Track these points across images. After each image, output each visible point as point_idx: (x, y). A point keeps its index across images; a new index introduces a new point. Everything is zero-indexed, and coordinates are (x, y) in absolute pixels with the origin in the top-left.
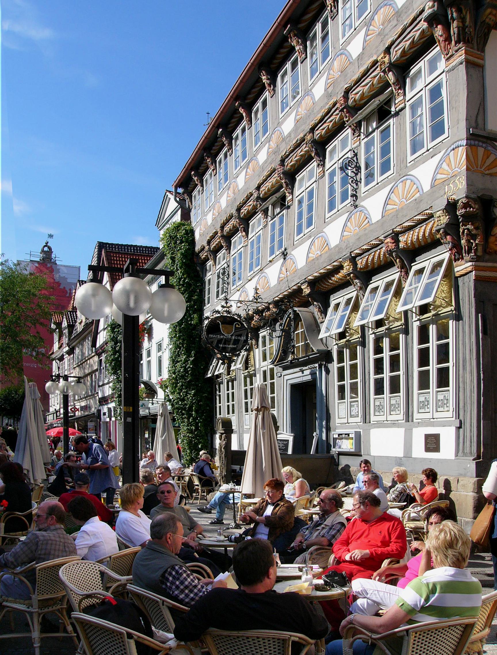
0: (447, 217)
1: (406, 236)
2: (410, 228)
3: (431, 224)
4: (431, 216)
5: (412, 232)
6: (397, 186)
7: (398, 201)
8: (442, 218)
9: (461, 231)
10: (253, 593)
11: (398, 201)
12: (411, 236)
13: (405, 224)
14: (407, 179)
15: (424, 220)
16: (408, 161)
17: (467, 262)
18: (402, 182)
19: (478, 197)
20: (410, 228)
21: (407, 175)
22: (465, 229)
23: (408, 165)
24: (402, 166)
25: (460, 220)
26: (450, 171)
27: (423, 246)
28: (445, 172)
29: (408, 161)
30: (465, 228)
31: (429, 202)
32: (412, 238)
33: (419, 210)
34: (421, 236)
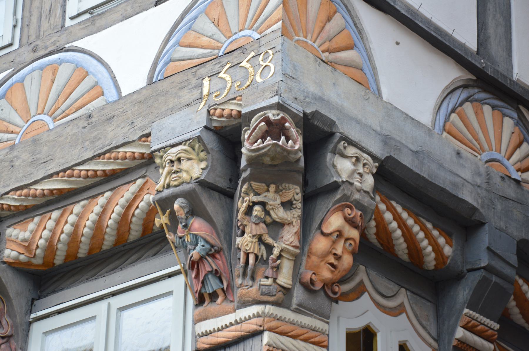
0: (203, 165)
1: (31, 226)
2: (60, 199)
3: (133, 188)
4: (148, 161)
5: (55, 214)
6: (22, 80)
7: (18, 120)
8: (185, 165)
9: (242, 206)
10: (454, 193)
11: (18, 120)
12: (50, 224)
13: (91, 166)
14: (61, 62)
15: (110, 177)
16: (71, 11)
17: (244, 304)
18: (42, 69)
19: (304, 113)
20: (60, 199)
21: (62, 50)
22: (254, 204)
23: (68, 23)
24: (45, 25)
25: (244, 175)
26: (223, 38)
27: (81, 260)
28: (204, 40)
29: (71, 11)
30: (256, 199)
31: (139, 123)
32: (53, 231)
33: (99, 144)
34: (88, 223)
